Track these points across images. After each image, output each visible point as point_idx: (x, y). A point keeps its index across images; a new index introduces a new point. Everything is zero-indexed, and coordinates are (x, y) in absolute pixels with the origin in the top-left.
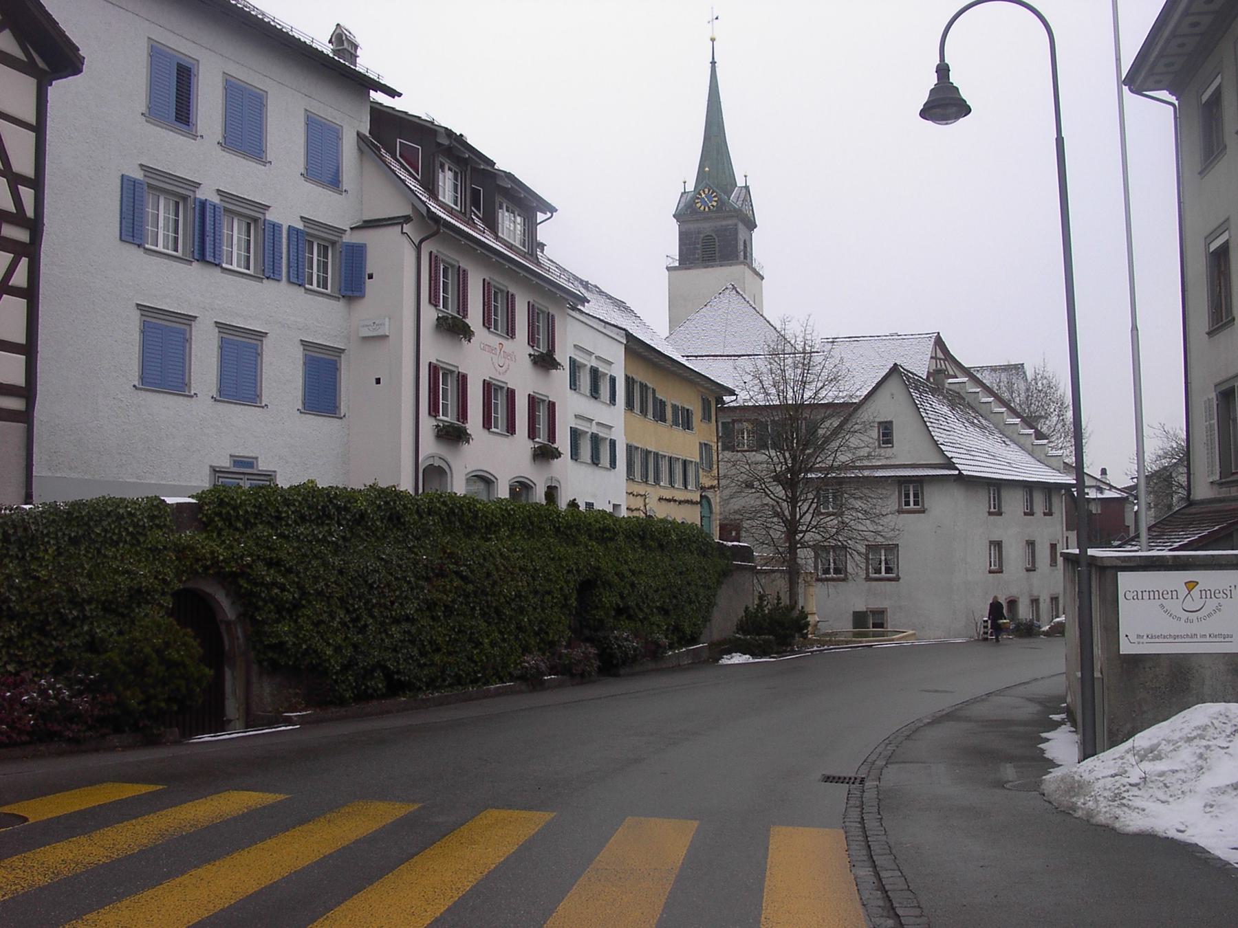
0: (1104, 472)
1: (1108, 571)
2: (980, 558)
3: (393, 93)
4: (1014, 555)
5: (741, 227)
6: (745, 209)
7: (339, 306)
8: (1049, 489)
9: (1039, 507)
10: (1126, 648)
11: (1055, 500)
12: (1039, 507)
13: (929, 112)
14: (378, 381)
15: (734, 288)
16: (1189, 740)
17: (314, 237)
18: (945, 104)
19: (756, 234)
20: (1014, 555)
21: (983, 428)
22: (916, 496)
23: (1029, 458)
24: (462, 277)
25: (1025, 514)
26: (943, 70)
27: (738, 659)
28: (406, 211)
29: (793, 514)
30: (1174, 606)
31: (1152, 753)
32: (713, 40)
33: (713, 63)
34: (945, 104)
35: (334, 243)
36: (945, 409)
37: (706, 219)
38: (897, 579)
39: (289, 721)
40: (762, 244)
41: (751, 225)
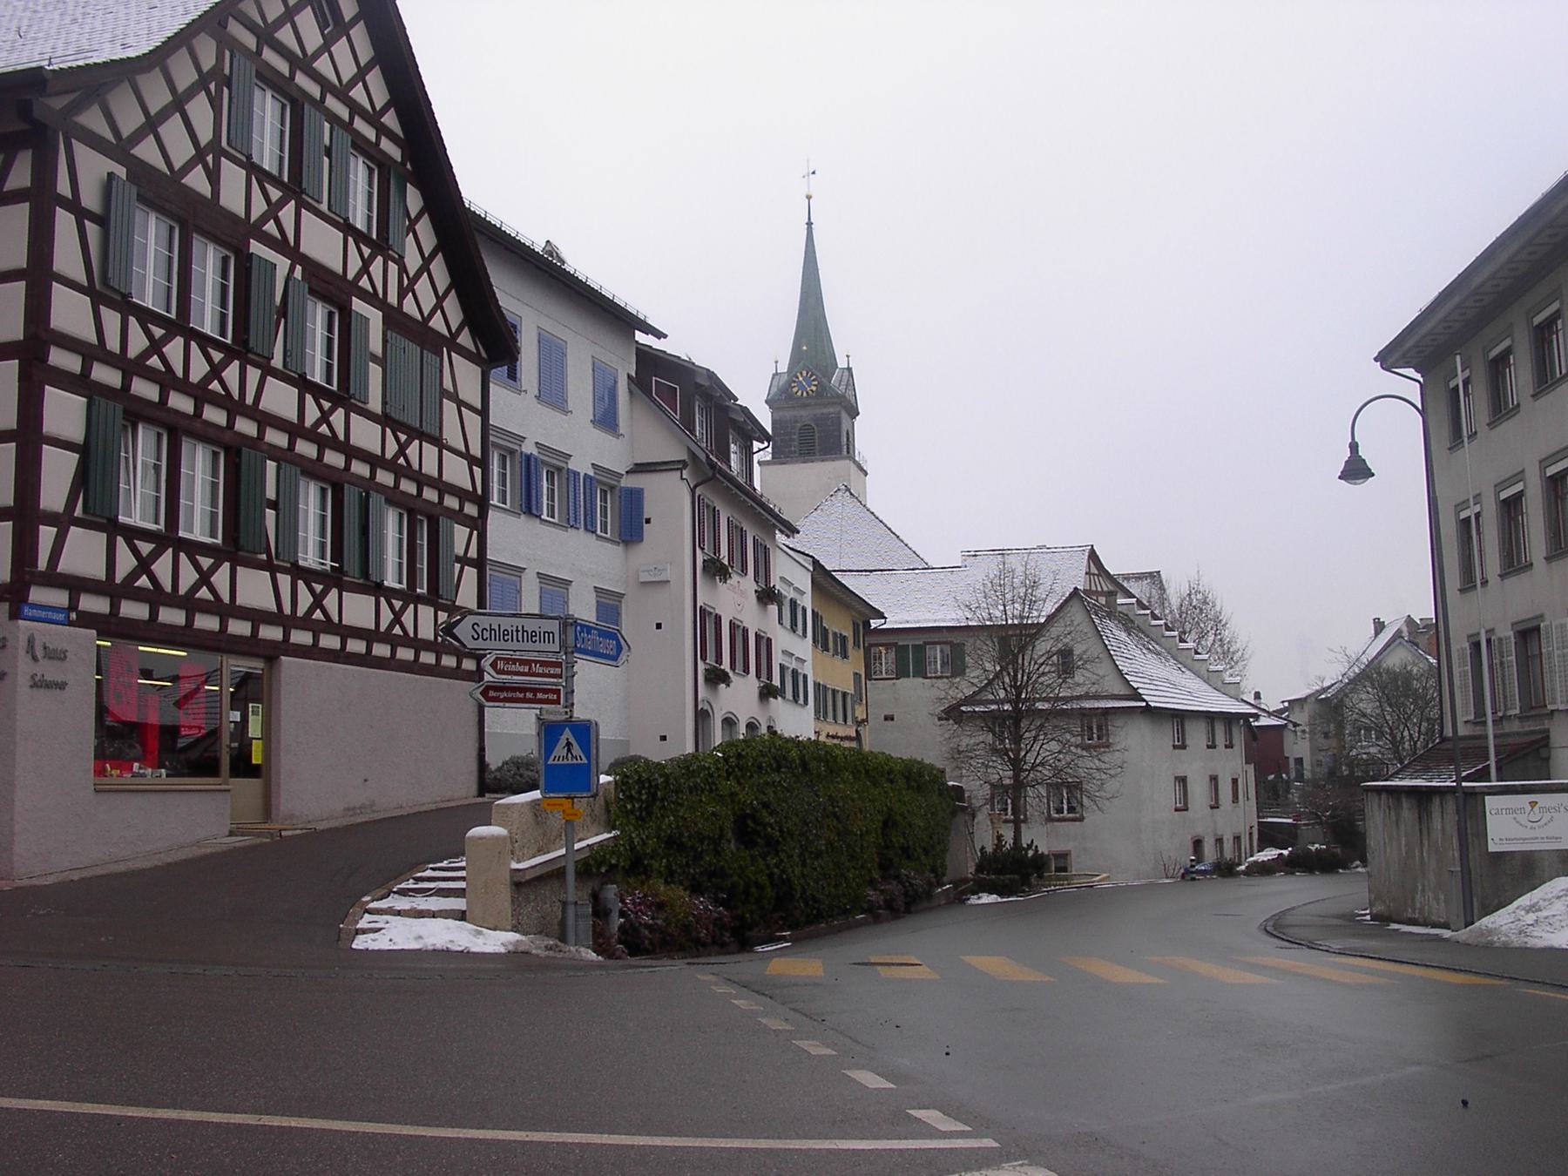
0: (1257, 696)
1: (1476, 797)
2: (1167, 794)
3: (659, 335)
4: (1199, 792)
5: (844, 415)
6: (849, 394)
7: (619, 549)
8: (1229, 719)
9: (1220, 739)
10: (1492, 848)
11: (1235, 731)
12: (1220, 739)
13: (1344, 476)
14: (659, 626)
15: (848, 490)
16: (1559, 897)
17: (602, 481)
18: (1356, 470)
19: (858, 421)
20: (1199, 792)
21: (1158, 654)
22: (1099, 728)
23: (1205, 686)
24: (715, 514)
25: (1175, 747)
26: (1354, 447)
27: (987, 899)
28: (682, 455)
29: (1017, 752)
30: (1523, 818)
31: (1532, 908)
32: (809, 197)
33: (809, 224)
34: (1356, 470)
35: (612, 488)
36: (1123, 636)
37: (805, 406)
38: (1081, 819)
39: (784, 939)
40: (866, 434)
41: (854, 413)
